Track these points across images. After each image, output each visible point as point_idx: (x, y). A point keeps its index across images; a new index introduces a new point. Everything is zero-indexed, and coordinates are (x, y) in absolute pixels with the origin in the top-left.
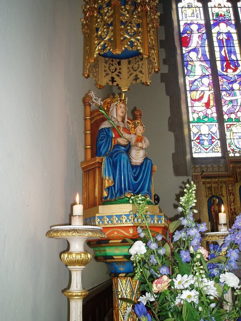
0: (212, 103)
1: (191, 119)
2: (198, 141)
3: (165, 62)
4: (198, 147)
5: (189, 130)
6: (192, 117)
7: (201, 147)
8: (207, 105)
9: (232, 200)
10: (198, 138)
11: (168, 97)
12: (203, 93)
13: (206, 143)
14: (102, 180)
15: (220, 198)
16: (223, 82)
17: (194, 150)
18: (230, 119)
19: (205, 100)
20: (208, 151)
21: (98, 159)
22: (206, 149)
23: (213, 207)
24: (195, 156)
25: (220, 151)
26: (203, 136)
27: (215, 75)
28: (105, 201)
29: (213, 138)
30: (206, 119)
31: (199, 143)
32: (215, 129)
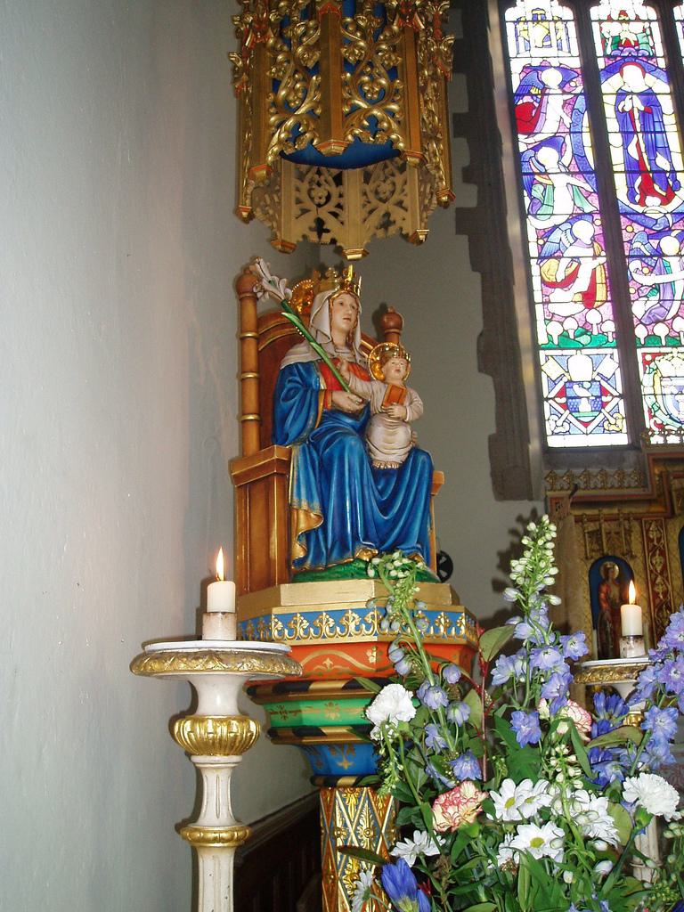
0: (601, 293)
1: (542, 339)
2: (563, 400)
3: (468, 176)
4: (563, 418)
5: (538, 369)
6: (546, 331)
7: (571, 418)
8: (589, 298)
9: (659, 569)
10: (562, 393)
11: (477, 277)
12: (575, 265)
13: (585, 406)
14: (289, 512)
15: (626, 563)
16: (632, 233)
17: (549, 427)
18: (652, 339)
19: (582, 284)
20: (590, 428)
21: (278, 453)
22: (586, 424)
23: (604, 589)
24: (553, 442)
25: (625, 430)
26: (576, 387)
27: (610, 212)
28: (297, 572)
29: (604, 392)
30: (585, 339)
31: (565, 406)
32: (610, 366)
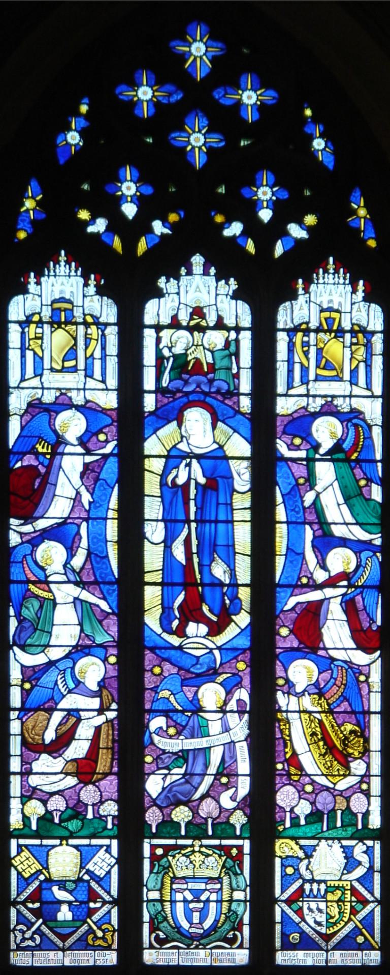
10: (36, 896)
19: (78, 749)
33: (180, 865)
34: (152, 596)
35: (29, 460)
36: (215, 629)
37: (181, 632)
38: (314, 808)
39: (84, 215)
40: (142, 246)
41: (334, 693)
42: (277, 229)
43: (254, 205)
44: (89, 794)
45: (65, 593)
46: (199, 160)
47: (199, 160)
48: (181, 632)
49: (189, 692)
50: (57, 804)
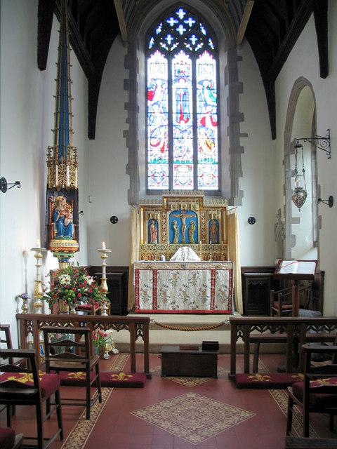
0: (166, 148)
1: (149, 161)
3: (127, 121)
5: (147, 168)
6: (150, 159)
8: (162, 150)
10: (153, 175)
13: (158, 179)
17: (149, 184)
19: (161, 145)
24: (149, 188)
27: (170, 125)
32: (166, 168)
33: (180, 169)
34: (174, 116)
35: (151, 89)
36: (186, 122)
37: (179, 123)
38: (163, 215)
39: (185, 44)
40: (196, 49)
41: (208, 135)
42: (196, 46)
43: (191, 41)
44: (163, 155)
45: (158, 115)
46: (182, 33)
47: (182, 33)
48: (179, 123)
49: (181, 134)
50: (157, 158)
